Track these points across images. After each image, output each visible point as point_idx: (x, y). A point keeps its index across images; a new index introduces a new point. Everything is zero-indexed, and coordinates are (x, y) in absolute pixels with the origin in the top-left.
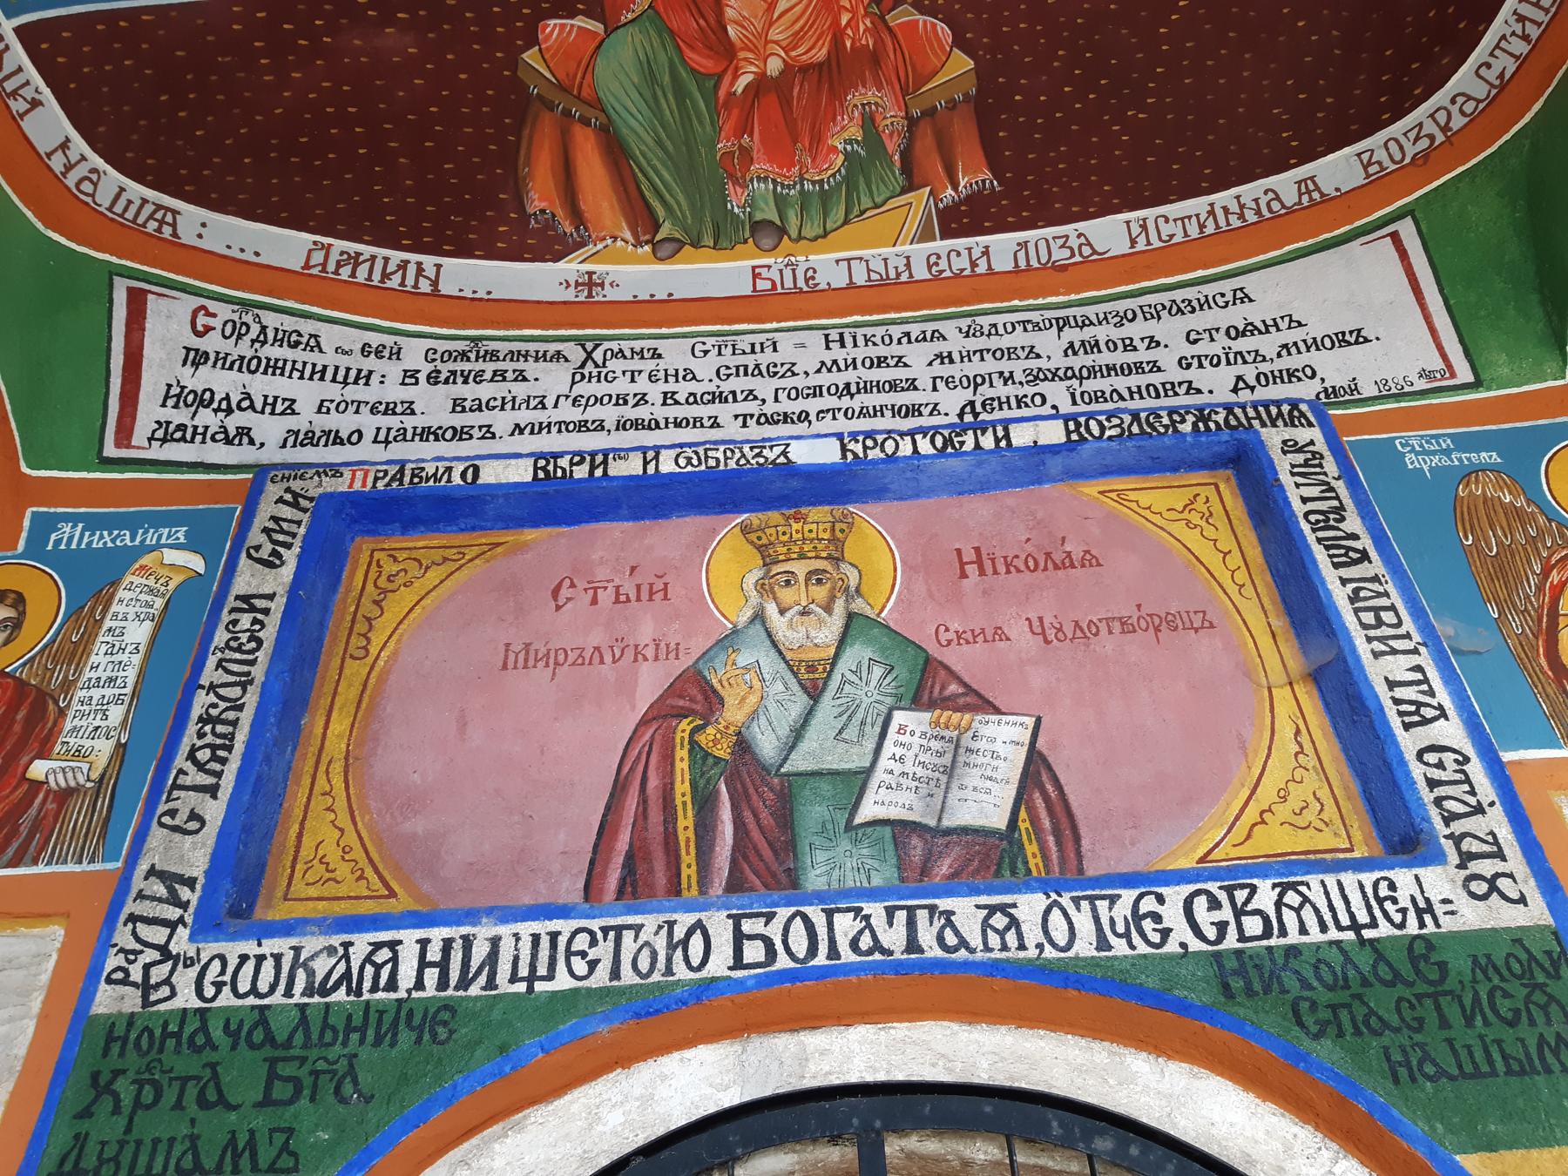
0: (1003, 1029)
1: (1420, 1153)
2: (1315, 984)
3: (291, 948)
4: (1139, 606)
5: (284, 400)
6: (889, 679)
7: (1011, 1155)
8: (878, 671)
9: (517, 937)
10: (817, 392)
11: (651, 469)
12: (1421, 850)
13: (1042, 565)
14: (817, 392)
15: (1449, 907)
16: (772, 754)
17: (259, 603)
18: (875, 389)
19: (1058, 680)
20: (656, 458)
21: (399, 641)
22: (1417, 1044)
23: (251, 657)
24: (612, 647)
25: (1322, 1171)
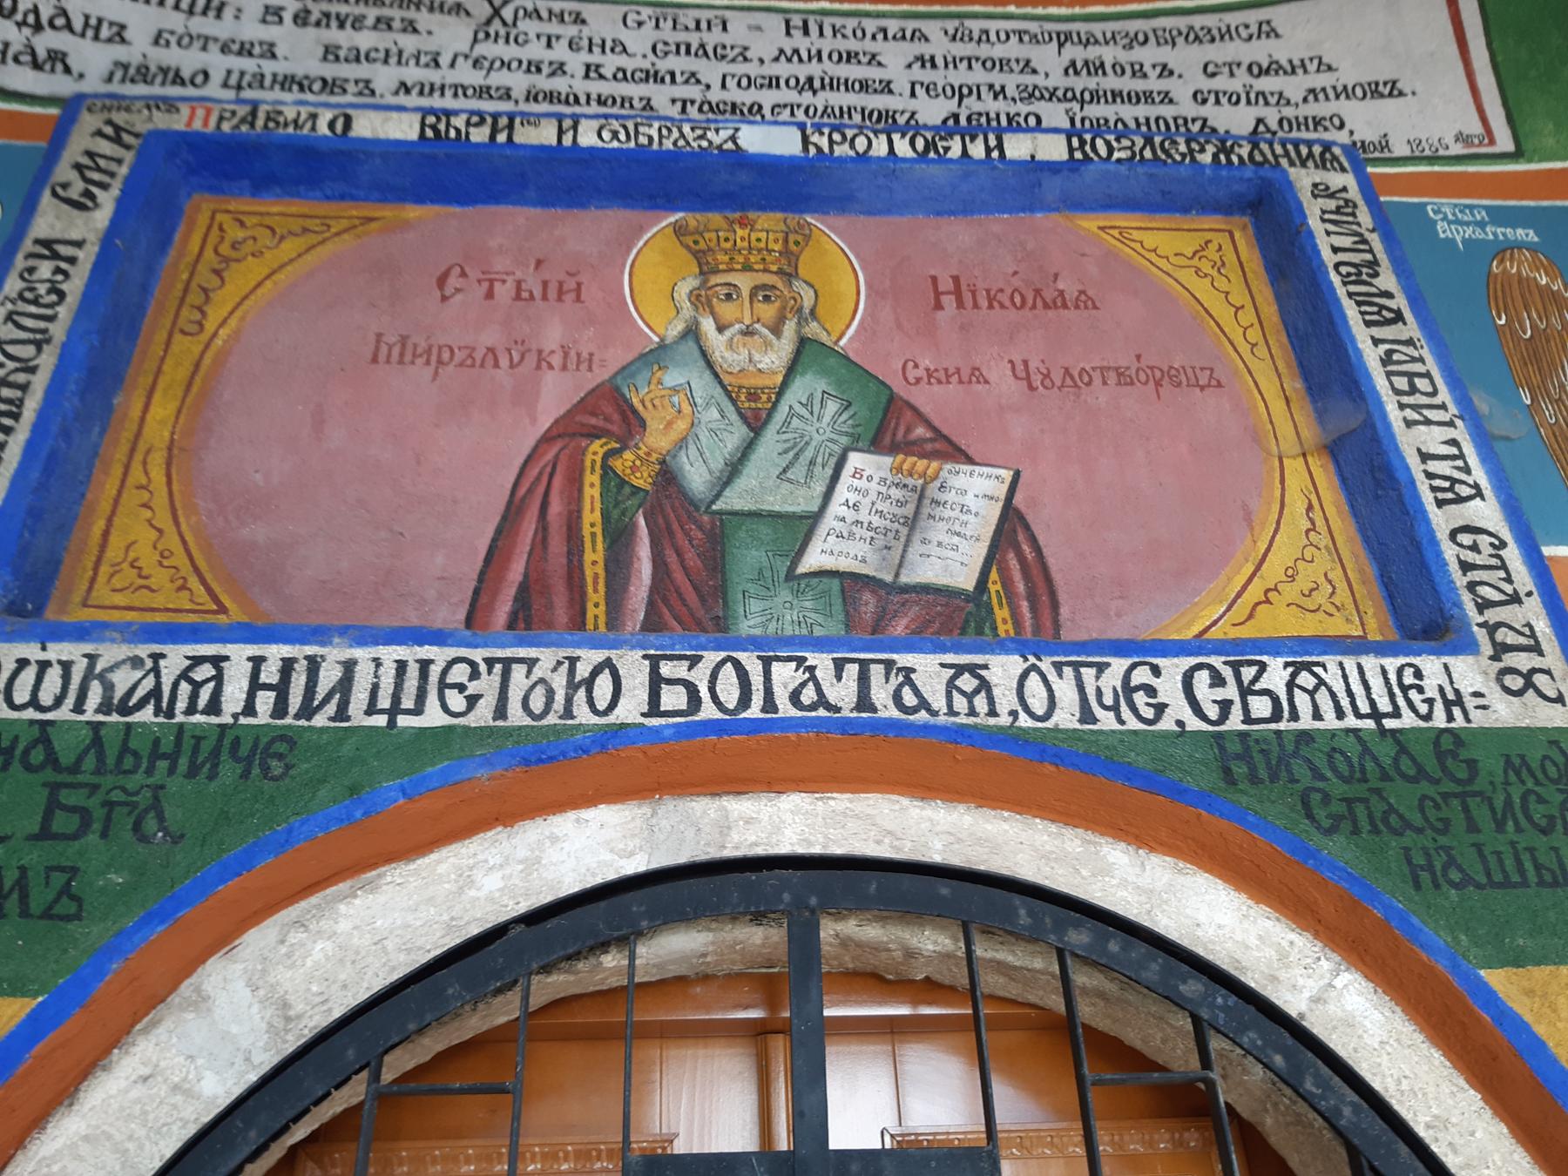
0: (961, 808)
1: (1442, 966)
2: (1329, 774)
3: (85, 656)
4: (1138, 357)
5: (111, 24)
6: (845, 416)
7: (969, 944)
8: (832, 407)
9: (377, 662)
10: (773, 83)
11: (567, 140)
12: (1451, 637)
13: (1030, 302)
14: (773, 83)
15: (1480, 701)
16: (701, 489)
17: (63, 250)
18: (842, 88)
19: (1042, 431)
20: (575, 128)
21: (242, 319)
22: (1441, 847)
23: (49, 312)
24: (509, 351)
25: (1322, 983)
